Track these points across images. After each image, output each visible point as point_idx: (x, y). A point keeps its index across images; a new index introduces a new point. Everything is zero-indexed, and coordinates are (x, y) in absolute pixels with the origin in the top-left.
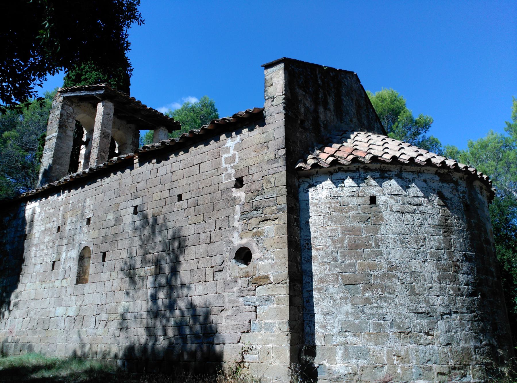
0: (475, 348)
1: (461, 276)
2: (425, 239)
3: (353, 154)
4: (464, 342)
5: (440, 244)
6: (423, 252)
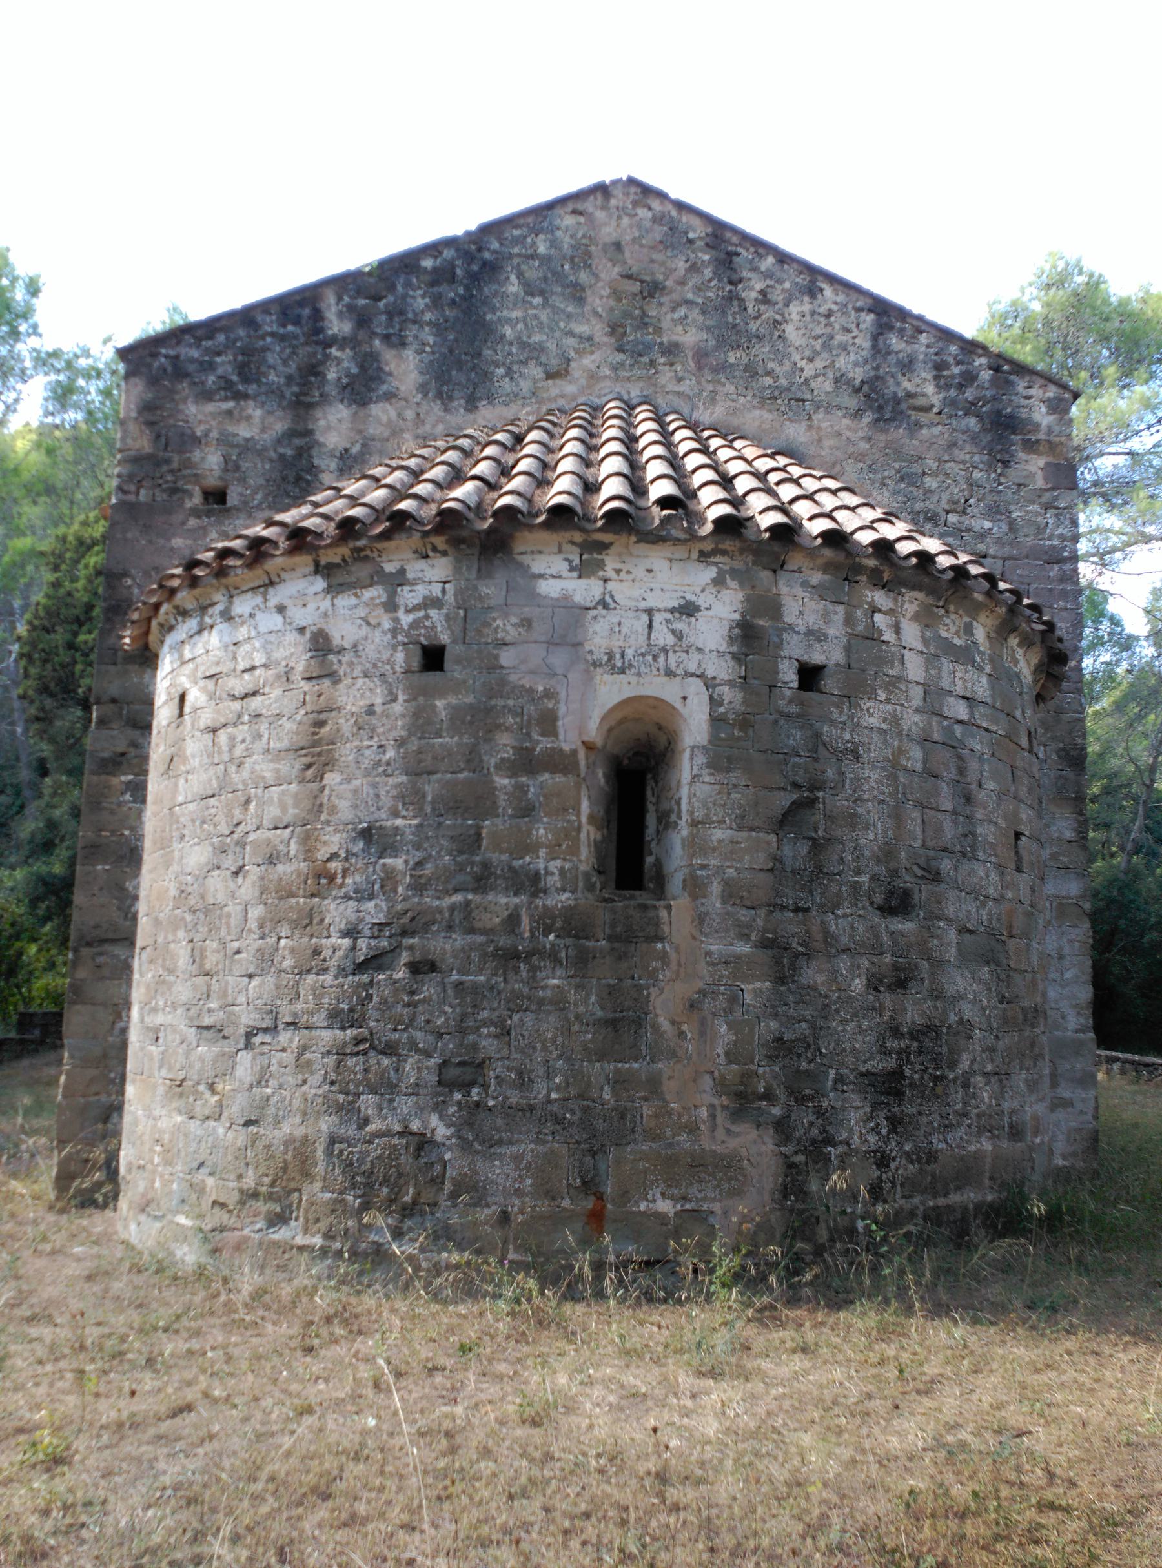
0: (333, 1140)
1: (332, 906)
2: (248, 801)
3: (834, 519)
4: (298, 1120)
5: (284, 809)
6: (237, 843)
